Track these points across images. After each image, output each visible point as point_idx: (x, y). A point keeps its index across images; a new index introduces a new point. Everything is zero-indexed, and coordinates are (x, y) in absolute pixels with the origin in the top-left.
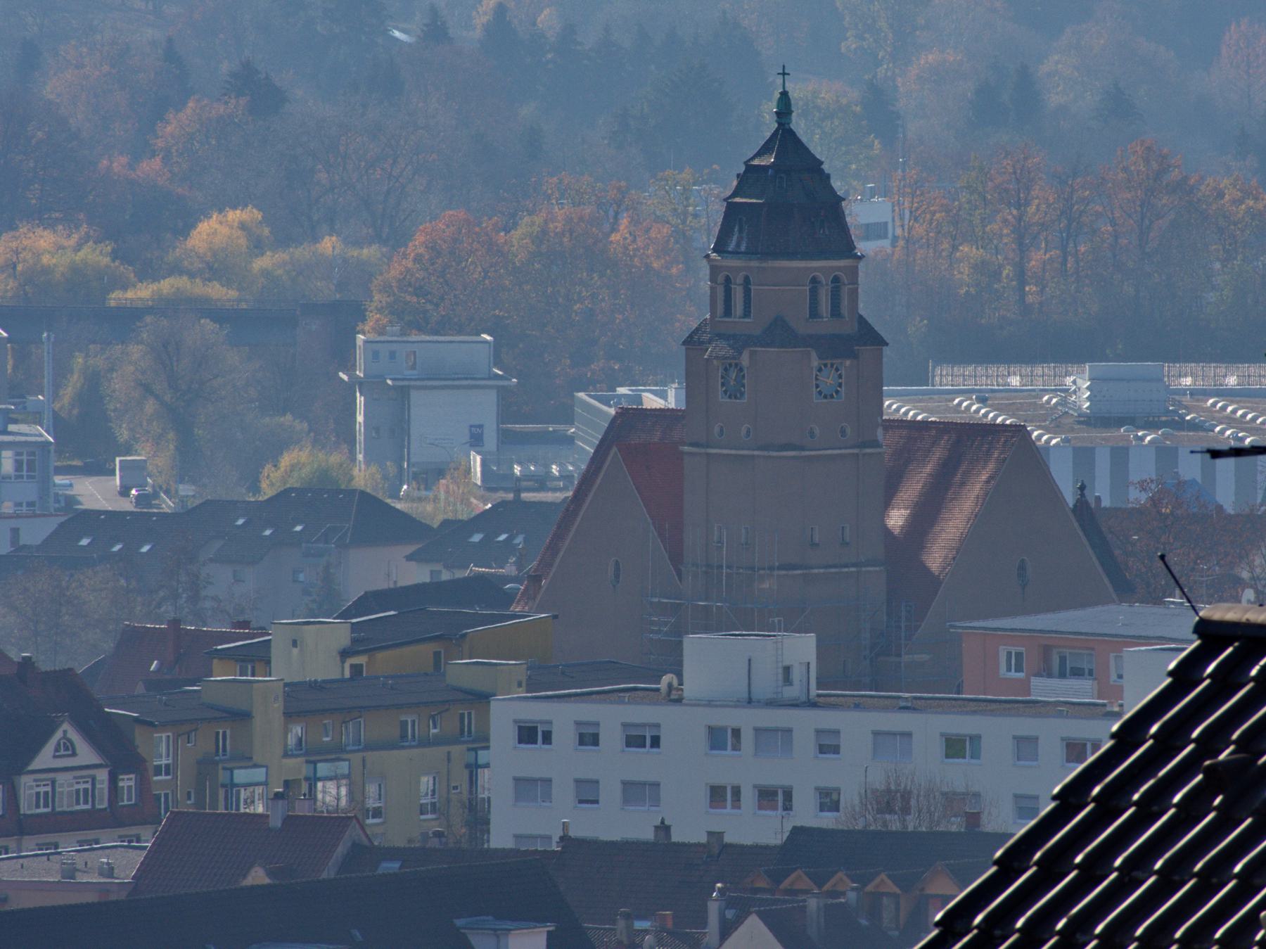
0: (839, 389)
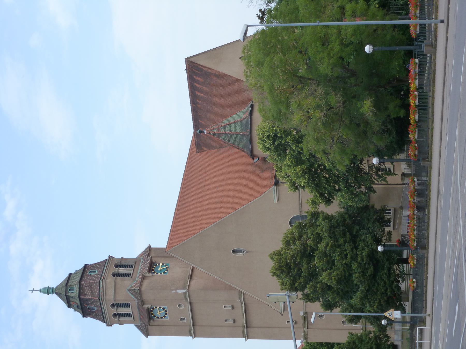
0: (156, 317)
